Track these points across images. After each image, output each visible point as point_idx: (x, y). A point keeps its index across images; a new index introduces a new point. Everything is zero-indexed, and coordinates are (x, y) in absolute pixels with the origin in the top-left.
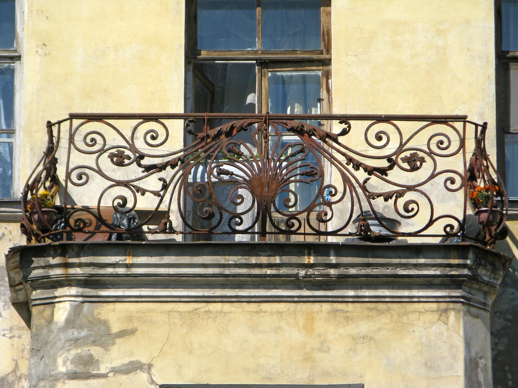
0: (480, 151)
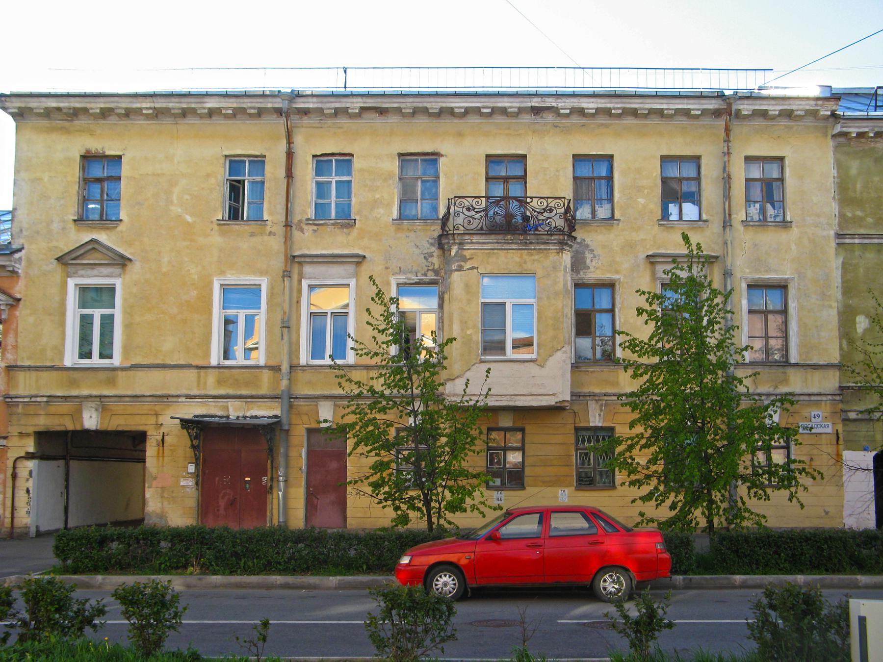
0: (568, 206)
